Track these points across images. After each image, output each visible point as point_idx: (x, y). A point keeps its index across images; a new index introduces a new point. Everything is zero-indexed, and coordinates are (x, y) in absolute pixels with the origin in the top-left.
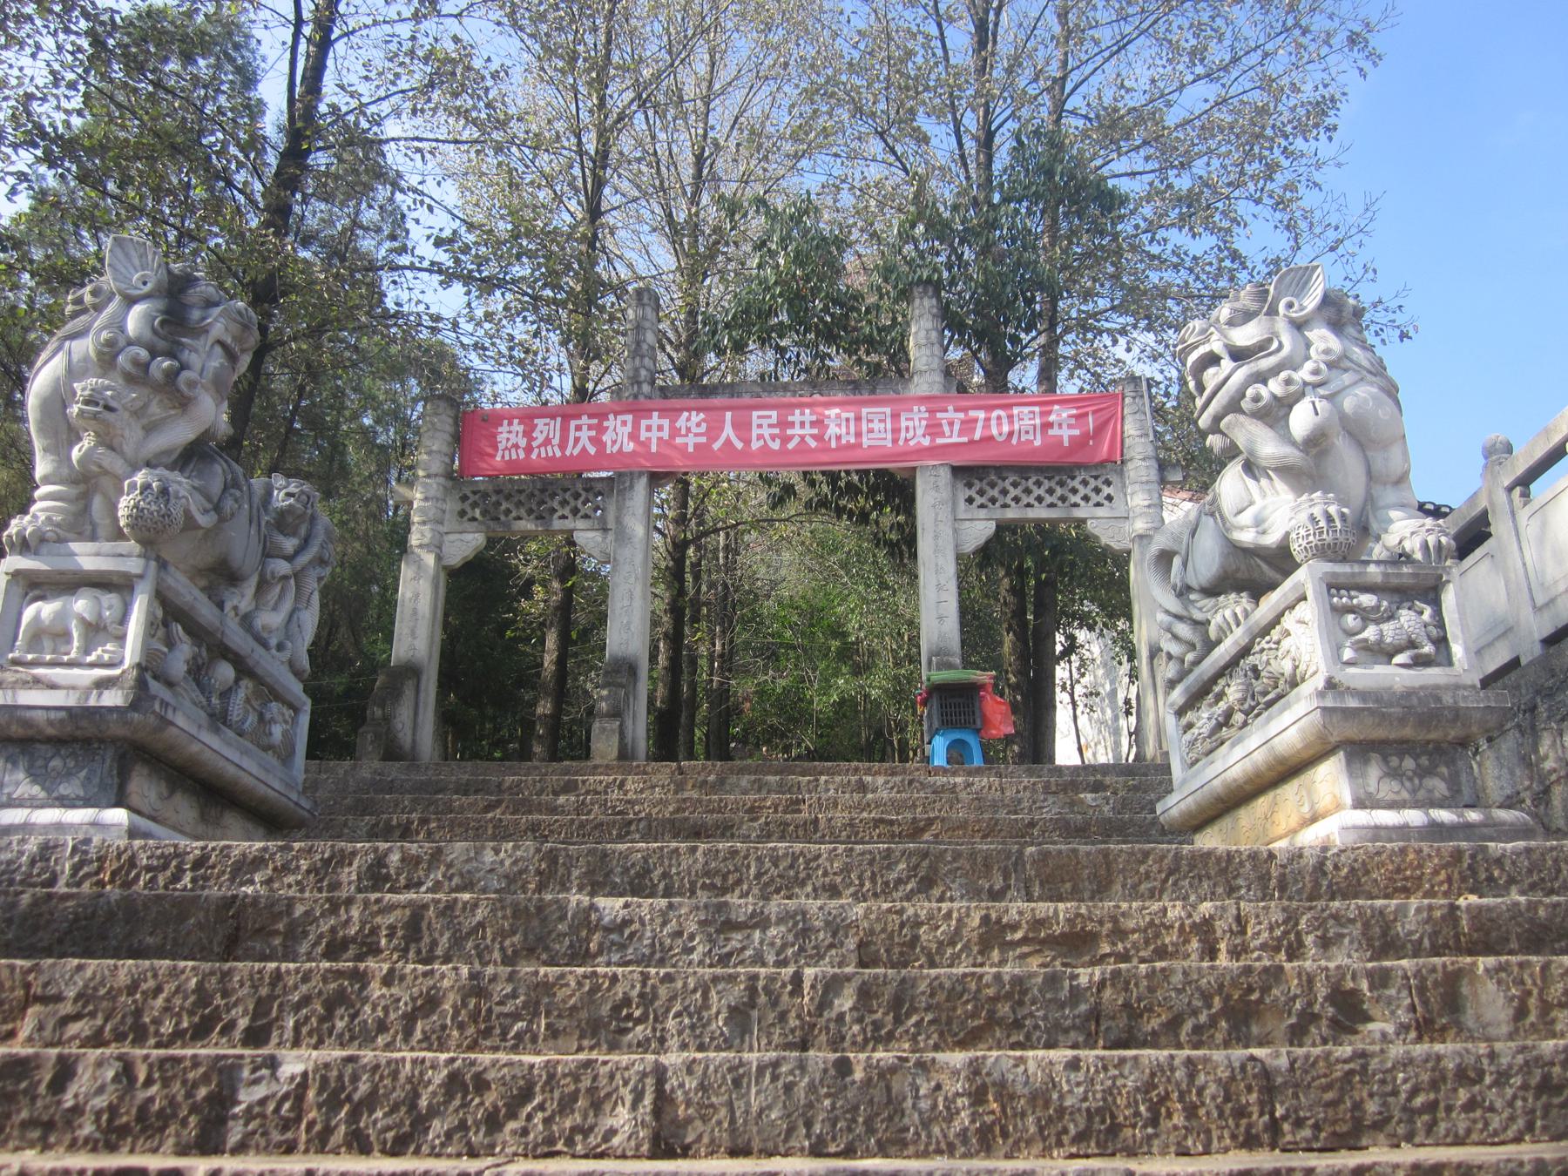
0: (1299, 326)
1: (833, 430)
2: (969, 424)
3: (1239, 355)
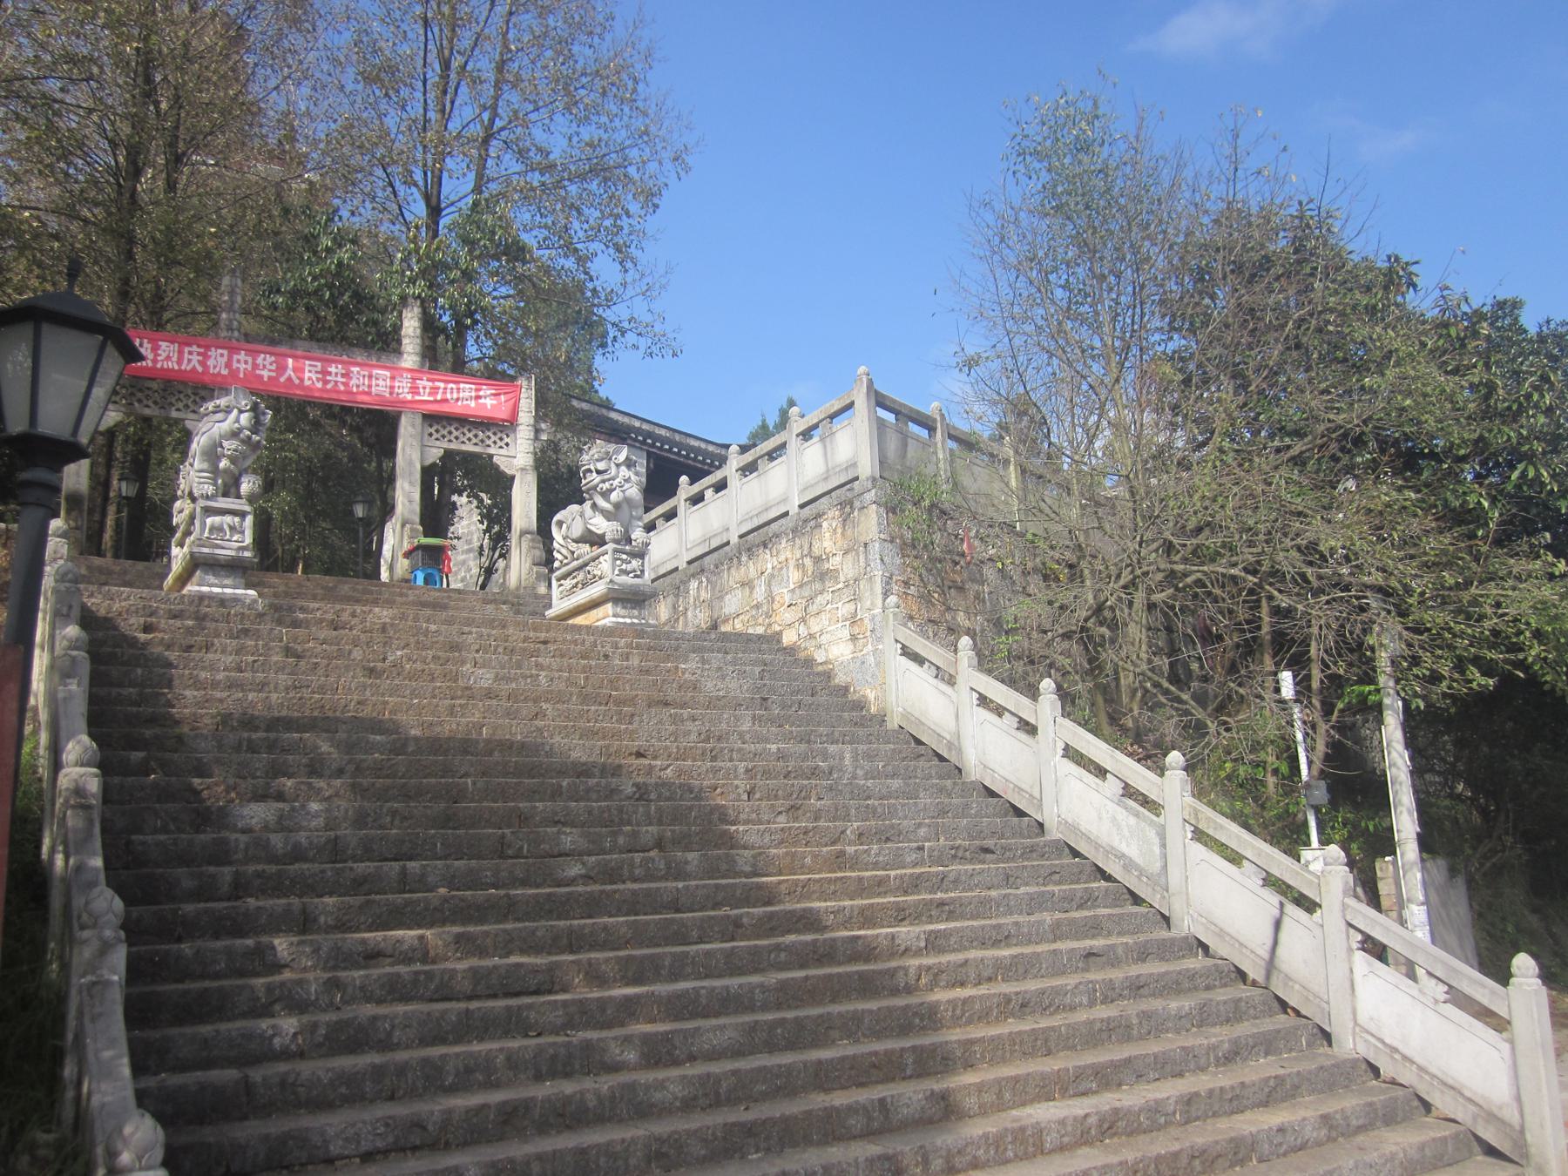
0: (618, 466)
1: (353, 382)
2: (435, 390)
3: (599, 472)
